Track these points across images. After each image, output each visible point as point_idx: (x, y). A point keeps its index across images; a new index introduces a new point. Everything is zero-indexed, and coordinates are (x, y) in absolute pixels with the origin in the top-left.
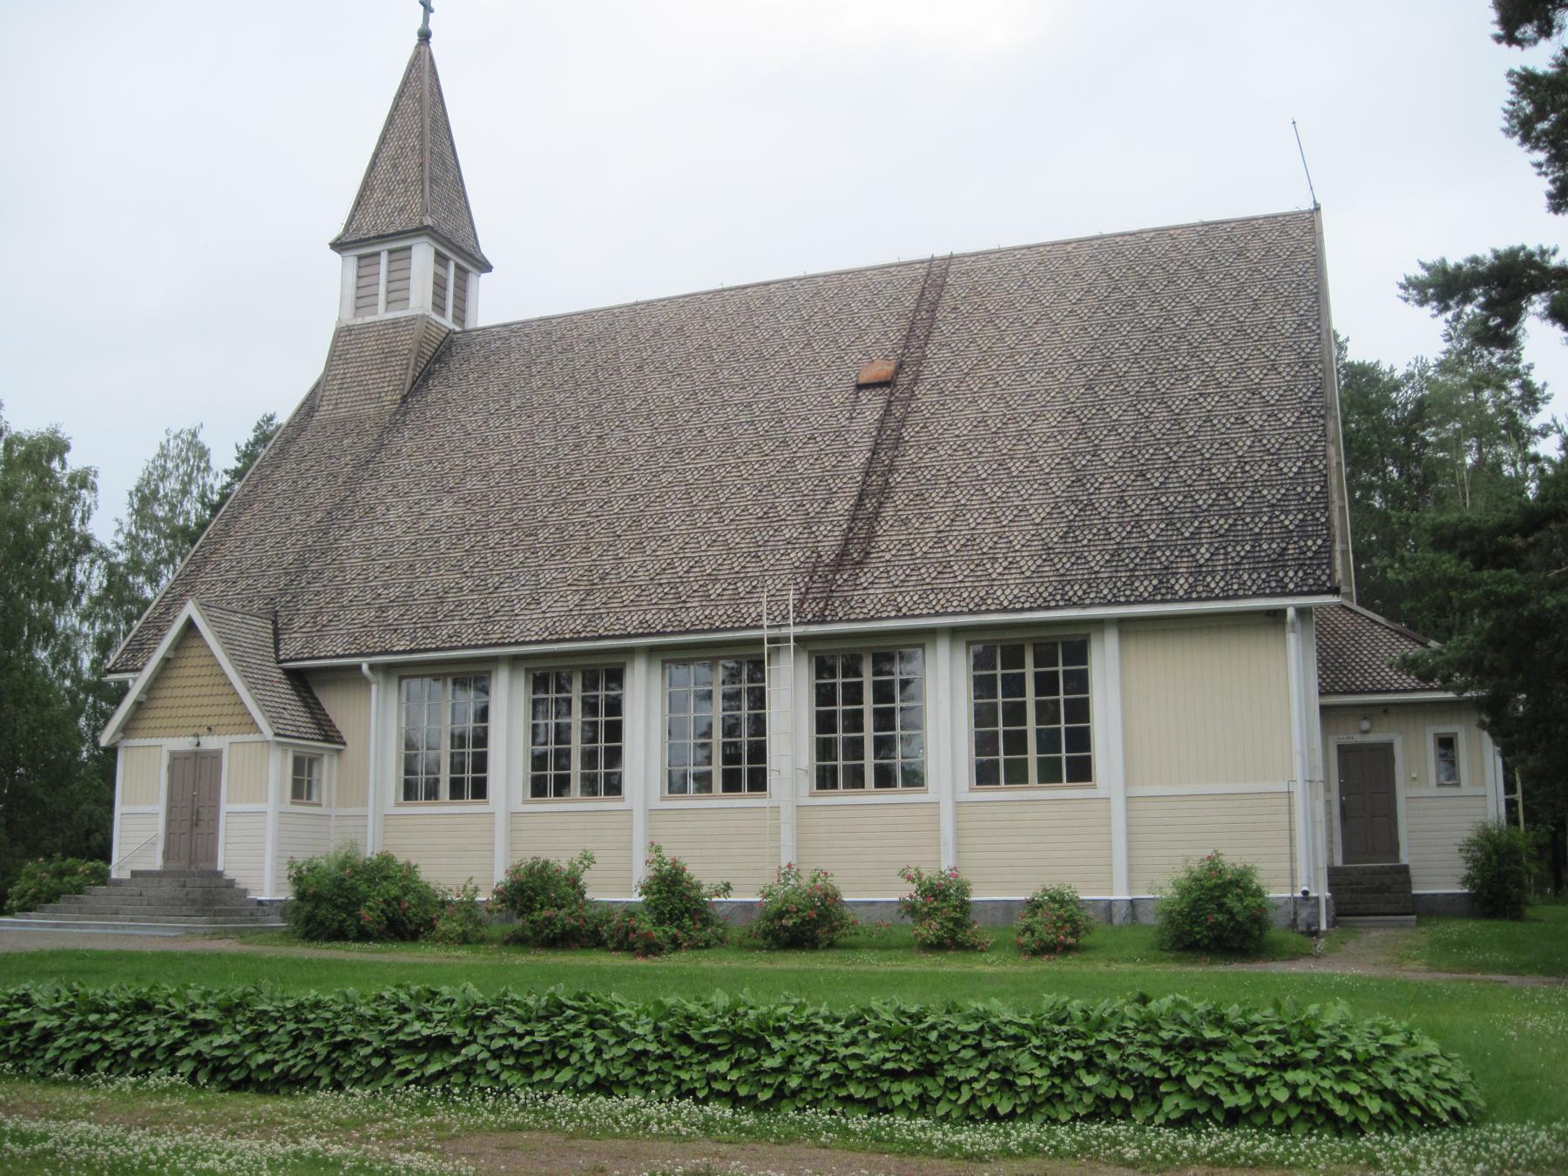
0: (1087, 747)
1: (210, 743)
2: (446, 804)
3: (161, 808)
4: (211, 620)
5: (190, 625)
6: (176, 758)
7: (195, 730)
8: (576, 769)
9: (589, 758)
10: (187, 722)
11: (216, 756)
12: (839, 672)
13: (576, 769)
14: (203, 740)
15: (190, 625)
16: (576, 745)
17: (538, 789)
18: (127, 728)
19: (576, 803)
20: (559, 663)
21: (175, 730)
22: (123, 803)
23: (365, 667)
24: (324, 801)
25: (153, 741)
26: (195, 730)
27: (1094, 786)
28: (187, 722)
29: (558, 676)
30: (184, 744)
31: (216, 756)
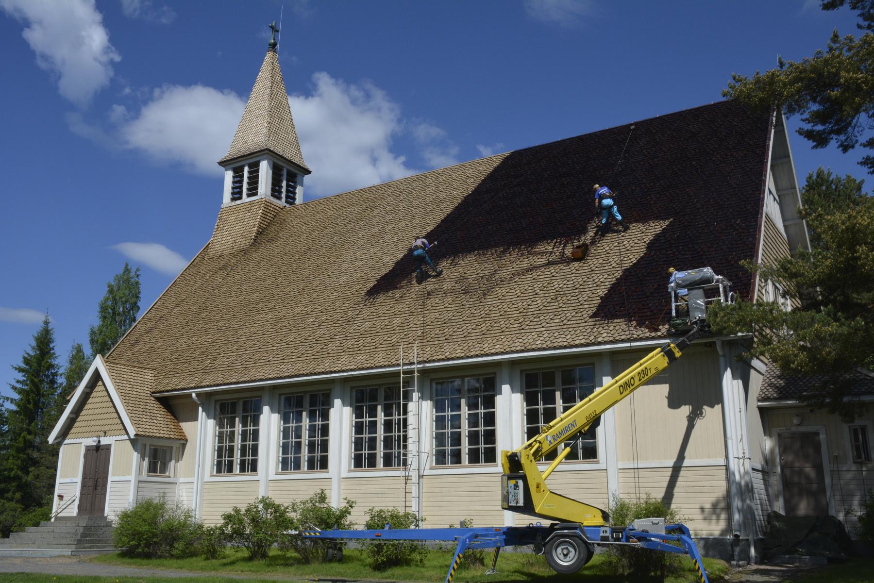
0: (494, 442)
1: (104, 441)
2: (304, 473)
3: (79, 479)
4: (110, 371)
5: (97, 372)
6: (88, 449)
7: (97, 434)
8: (465, 446)
9: (474, 438)
10: (94, 429)
11: (108, 447)
12: (540, 382)
13: (465, 446)
14: (102, 439)
15: (97, 372)
16: (465, 429)
17: (358, 462)
18: (65, 433)
19: (380, 472)
20: (301, 389)
21: (87, 434)
22: (61, 477)
23: (194, 395)
24: (172, 475)
25: (78, 441)
26: (97, 434)
27: (598, 462)
28: (94, 429)
29: (245, 403)
30: (91, 442)
31: (108, 447)
